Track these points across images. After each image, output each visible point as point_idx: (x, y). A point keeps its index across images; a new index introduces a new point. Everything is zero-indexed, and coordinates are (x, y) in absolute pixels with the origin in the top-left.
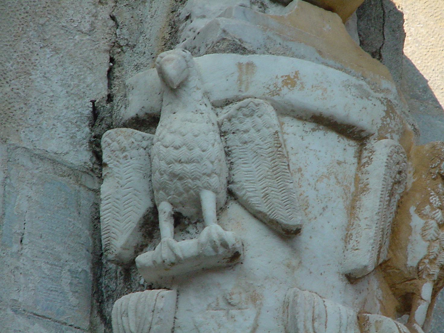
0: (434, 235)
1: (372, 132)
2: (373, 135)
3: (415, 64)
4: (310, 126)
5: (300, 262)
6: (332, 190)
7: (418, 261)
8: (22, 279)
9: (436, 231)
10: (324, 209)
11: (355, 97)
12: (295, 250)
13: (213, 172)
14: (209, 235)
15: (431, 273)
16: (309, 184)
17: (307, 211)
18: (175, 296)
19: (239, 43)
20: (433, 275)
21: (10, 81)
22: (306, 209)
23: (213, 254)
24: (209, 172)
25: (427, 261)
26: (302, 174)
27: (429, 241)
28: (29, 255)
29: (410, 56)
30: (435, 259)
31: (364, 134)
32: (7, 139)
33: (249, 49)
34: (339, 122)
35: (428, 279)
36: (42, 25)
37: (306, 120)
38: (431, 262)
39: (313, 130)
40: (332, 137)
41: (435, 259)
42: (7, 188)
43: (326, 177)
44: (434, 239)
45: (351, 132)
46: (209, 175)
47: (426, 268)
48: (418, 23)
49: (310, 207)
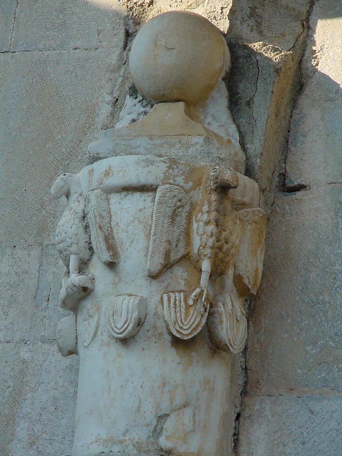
0: (202, 231)
1: (158, 184)
2: (159, 185)
3: (331, 77)
4: (124, 194)
5: (120, 279)
6: (136, 229)
7: (197, 249)
8: (48, 322)
9: (203, 228)
10: (132, 242)
11: (143, 168)
12: (117, 273)
13: (72, 244)
14: (71, 281)
15: (205, 254)
16: (123, 230)
17: (122, 247)
18: (75, 318)
19: (96, 155)
20: (207, 254)
21: (46, 207)
22: (122, 246)
23: (72, 292)
24: (69, 244)
25: (201, 248)
26: (118, 226)
27: (200, 235)
28: (52, 307)
29: (327, 73)
30: (206, 245)
31: (154, 187)
32: (43, 243)
33: (102, 157)
34: (136, 186)
35: (205, 258)
36: (67, 165)
37: (121, 192)
38: (204, 247)
39: (126, 196)
40: (137, 195)
41: (206, 245)
42: (41, 272)
43: (132, 222)
44: (203, 233)
45: (147, 189)
46: (70, 246)
47: (202, 252)
48: (335, 47)
49: (124, 244)
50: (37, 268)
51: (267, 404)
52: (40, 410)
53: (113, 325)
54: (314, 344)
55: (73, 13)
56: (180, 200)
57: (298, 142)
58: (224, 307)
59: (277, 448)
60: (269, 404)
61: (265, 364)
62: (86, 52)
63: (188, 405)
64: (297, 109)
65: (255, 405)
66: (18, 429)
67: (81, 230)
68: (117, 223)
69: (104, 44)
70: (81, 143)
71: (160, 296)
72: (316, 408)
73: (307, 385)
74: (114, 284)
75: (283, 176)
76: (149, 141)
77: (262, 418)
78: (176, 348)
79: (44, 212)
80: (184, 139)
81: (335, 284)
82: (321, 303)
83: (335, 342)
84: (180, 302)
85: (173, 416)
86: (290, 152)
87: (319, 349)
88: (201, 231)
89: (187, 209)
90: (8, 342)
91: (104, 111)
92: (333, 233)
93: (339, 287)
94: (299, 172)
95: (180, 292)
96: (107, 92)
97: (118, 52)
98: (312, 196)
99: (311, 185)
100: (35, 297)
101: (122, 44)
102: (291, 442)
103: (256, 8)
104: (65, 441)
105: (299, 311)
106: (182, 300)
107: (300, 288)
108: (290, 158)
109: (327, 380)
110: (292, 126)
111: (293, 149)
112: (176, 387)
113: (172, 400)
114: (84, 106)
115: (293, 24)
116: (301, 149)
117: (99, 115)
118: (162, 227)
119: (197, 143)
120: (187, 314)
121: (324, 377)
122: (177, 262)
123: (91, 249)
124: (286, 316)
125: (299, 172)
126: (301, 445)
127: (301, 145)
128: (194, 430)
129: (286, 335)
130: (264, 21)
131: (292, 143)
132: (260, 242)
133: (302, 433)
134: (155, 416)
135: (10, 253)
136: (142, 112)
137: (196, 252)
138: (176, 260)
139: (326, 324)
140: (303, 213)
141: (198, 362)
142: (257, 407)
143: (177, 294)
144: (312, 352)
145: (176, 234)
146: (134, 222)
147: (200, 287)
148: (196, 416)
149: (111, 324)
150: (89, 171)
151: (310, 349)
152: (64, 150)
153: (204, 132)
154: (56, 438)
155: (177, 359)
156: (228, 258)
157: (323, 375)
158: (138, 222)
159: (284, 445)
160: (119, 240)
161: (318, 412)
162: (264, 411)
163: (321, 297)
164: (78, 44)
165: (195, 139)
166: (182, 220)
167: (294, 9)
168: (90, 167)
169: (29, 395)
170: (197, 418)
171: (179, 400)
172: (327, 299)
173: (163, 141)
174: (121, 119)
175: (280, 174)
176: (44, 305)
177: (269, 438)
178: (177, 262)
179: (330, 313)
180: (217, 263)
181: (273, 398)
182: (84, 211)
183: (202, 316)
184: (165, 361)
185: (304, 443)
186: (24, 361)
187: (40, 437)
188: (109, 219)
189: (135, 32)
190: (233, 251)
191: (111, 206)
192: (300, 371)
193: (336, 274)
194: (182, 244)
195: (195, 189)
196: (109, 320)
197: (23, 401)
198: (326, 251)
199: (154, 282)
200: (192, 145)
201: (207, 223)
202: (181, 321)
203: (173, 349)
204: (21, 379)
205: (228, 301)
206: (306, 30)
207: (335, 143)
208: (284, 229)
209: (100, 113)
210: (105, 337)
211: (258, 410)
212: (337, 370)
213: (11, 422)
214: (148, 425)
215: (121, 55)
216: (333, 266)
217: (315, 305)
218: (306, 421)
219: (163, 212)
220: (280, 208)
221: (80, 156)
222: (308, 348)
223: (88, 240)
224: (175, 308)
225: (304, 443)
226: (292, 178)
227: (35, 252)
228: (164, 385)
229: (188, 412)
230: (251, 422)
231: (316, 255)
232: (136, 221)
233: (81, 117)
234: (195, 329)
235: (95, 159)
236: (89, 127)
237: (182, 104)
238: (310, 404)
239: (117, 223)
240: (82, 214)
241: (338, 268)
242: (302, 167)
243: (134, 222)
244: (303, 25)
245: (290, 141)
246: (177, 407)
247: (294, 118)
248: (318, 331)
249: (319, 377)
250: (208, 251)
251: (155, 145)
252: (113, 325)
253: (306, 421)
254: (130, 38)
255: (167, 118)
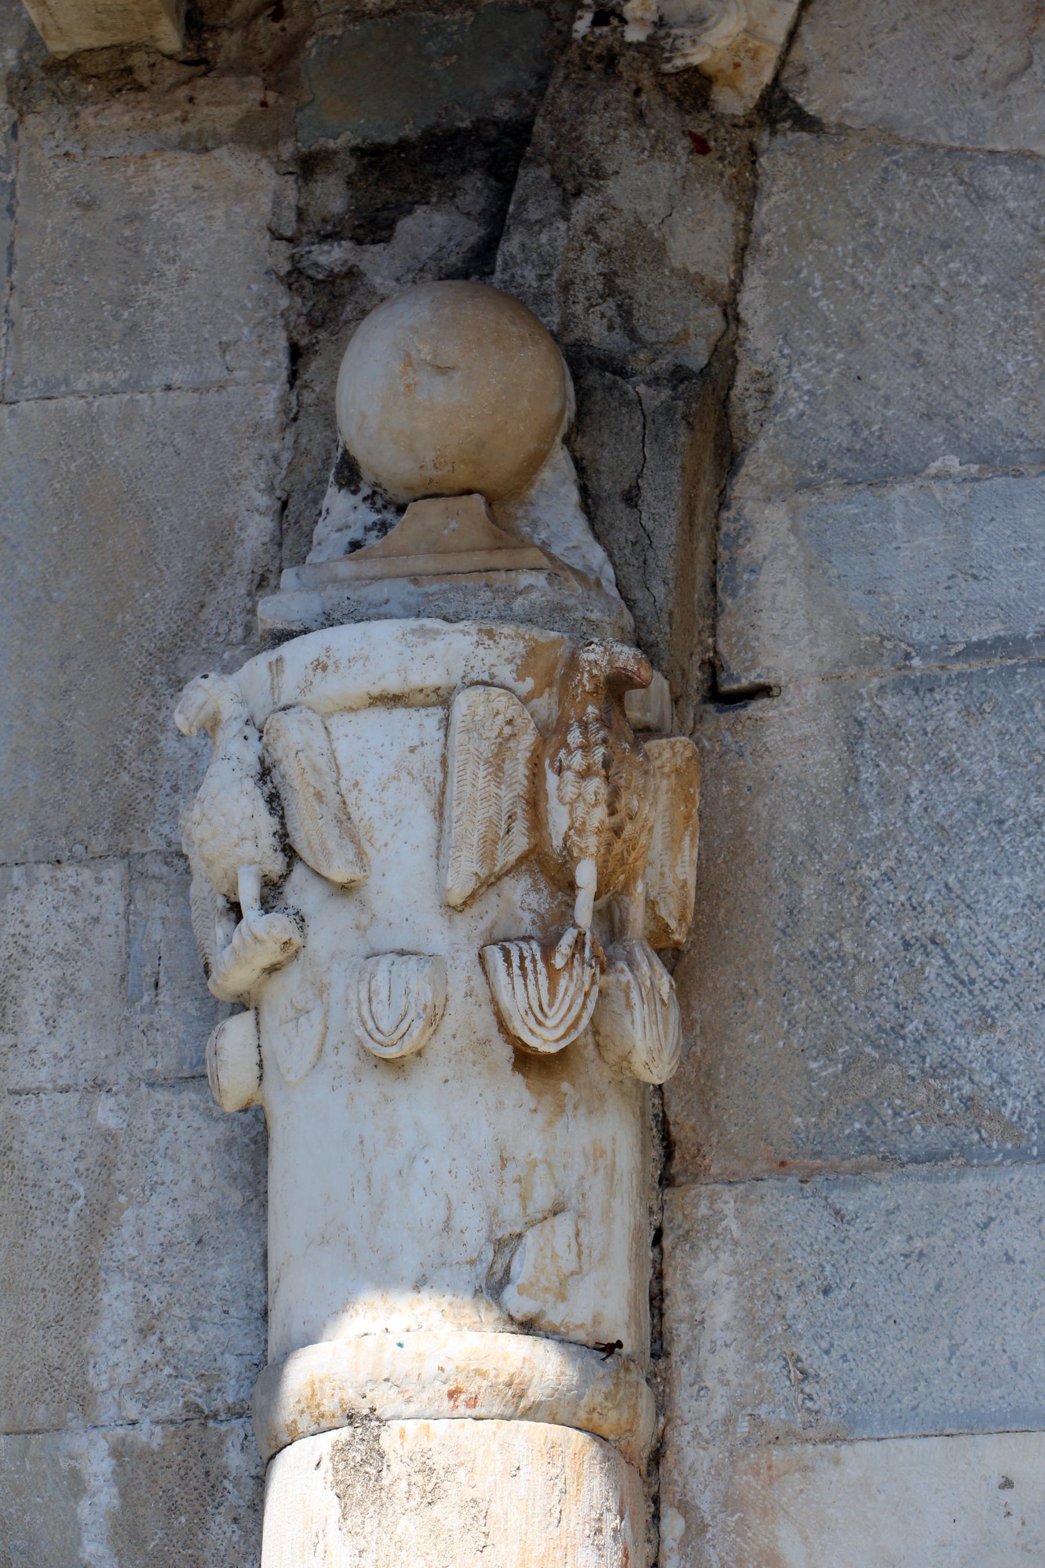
42: (131, 918)
50: (121, 909)
51: (726, 1202)
52: (159, 1249)
53: (370, 1025)
54: (827, 1051)
55: (153, 304)
56: (510, 722)
57: (741, 586)
58: (632, 971)
59: (763, 1306)
60: (732, 1201)
61: (712, 1109)
62: (196, 395)
63: (562, 1210)
64: (728, 507)
65: (696, 1206)
66: (106, 1298)
67: (262, 807)
68: (356, 784)
69: (239, 374)
70: (205, 610)
71: (476, 951)
72: (851, 1207)
73: (821, 1152)
74: (357, 927)
75: (713, 668)
76: (411, 587)
77: (718, 1235)
78: (523, 1074)
79: (125, 777)
80: (500, 579)
81: (864, 910)
82: (835, 956)
83: (878, 1047)
84: (534, 961)
85: (530, 1238)
86: (722, 611)
87: (840, 1066)
88: (570, 792)
89: (529, 743)
90: (65, 1090)
91: (252, 531)
92: (847, 792)
93: (874, 918)
94: (750, 654)
95: (527, 939)
96: (256, 487)
97: (275, 394)
98: (786, 710)
99: (782, 683)
100: (123, 979)
101: (284, 375)
102: (795, 1289)
103: (615, 273)
104: (229, 1321)
105: (784, 979)
106: (538, 957)
107: (780, 924)
108: (725, 623)
109: (868, 1139)
110: (720, 548)
111: (729, 601)
112: (533, 1165)
113: (524, 1198)
114: (202, 522)
115: (703, 312)
116: (749, 600)
117: (242, 541)
118: (473, 785)
119: (529, 588)
120: (552, 991)
121: (860, 1130)
122: (507, 873)
123: (290, 853)
124: (751, 992)
125: (750, 654)
126: (821, 1296)
127: (749, 590)
128: (581, 1267)
129: (757, 1037)
130: (636, 306)
131: (725, 589)
132: (688, 817)
133: (821, 1265)
134: (489, 1240)
135: (47, 878)
136: (375, 524)
137: (557, 842)
138: (508, 866)
139: (853, 1006)
140: (767, 750)
141: (576, 1107)
142: (703, 1210)
143: (524, 945)
144: (824, 1074)
145: (505, 805)
146: (399, 779)
147: (575, 926)
148: (582, 1235)
149: (364, 1023)
150: (270, 664)
151: (820, 1068)
152: (162, 629)
153: (545, 562)
154: (205, 1313)
155: (529, 1100)
156: (634, 855)
157: (857, 1125)
158: (408, 778)
159: (779, 1298)
160: (363, 823)
161: (856, 1213)
162: (722, 1220)
163: (833, 944)
164: (177, 377)
165: (525, 579)
166: (519, 771)
167: (703, 279)
168: (270, 656)
169: (129, 1214)
170: (584, 1239)
171: (542, 1197)
172: (849, 947)
173: (446, 586)
174: (319, 544)
175: (703, 663)
176: (146, 999)
177: (740, 1284)
178: (507, 873)
179: (859, 980)
180: (611, 866)
181: (741, 1187)
182: (262, 761)
183: (587, 995)
184: (500, 1105)
185: (826, 1292)
186: (108, 1136)
187: (166, 1314)
188: (334, 775)
189: (313, 345)
190: (643, 840)
191: (335, 744)
192: (798, 1120)
193: (864, 887)
194: (520, 826)
195: (541, 695)
196: (360, 1014)
197: (113, 1229)
198: (835, 835)
199: (457, 917)
200: (521, 593)
201: (585, 775)
202: (541, 1009)
203: (519, 1077)
204: (104, 1177)
205: (639, 955)
206: (733, 326)
207: (830, 585)
208: (725, 789)
209: (243, 536)
210: (347, 1058)
211: (706, 1218)
212: (890, 1112)
213: (89, 1283)
214: (472, 1262)
215: (283, 400)
216: (854, 868)
217: (820, 963)
218: (827, 1238)
219: (473, 750)
220: (710, 740)
221: (204, 640)
222: (813, 1065)
223: (278, 827)
224: (524, 976)
225: (826, 1292)
226: (735, 668)
227: (114, 872)
228: (504, 1162)
229: (564, 1225)
230: (692, 1248)
231: (812, 847)
232: (404, 776)
233: (199, 547)
234: (574, 1025)
235: (281, 637)
236: (222, 572)
237: (477, 499)
238: (832, 1196)
239: (356, 784)
240: (258, 768)
241: (867, 873)
242: (755, 644)
243: (399, 779)
244: (725, 315)
245: (720, 584)
246: (539, 1216)
247: (724, 529)
248: (833, 1023)
249: (847, 1132)
250: (592, 843)
251: (427, 595)
252: (370, 1025)
253: (827, 1238)
254: (301, 361)
255: (446, 532)
